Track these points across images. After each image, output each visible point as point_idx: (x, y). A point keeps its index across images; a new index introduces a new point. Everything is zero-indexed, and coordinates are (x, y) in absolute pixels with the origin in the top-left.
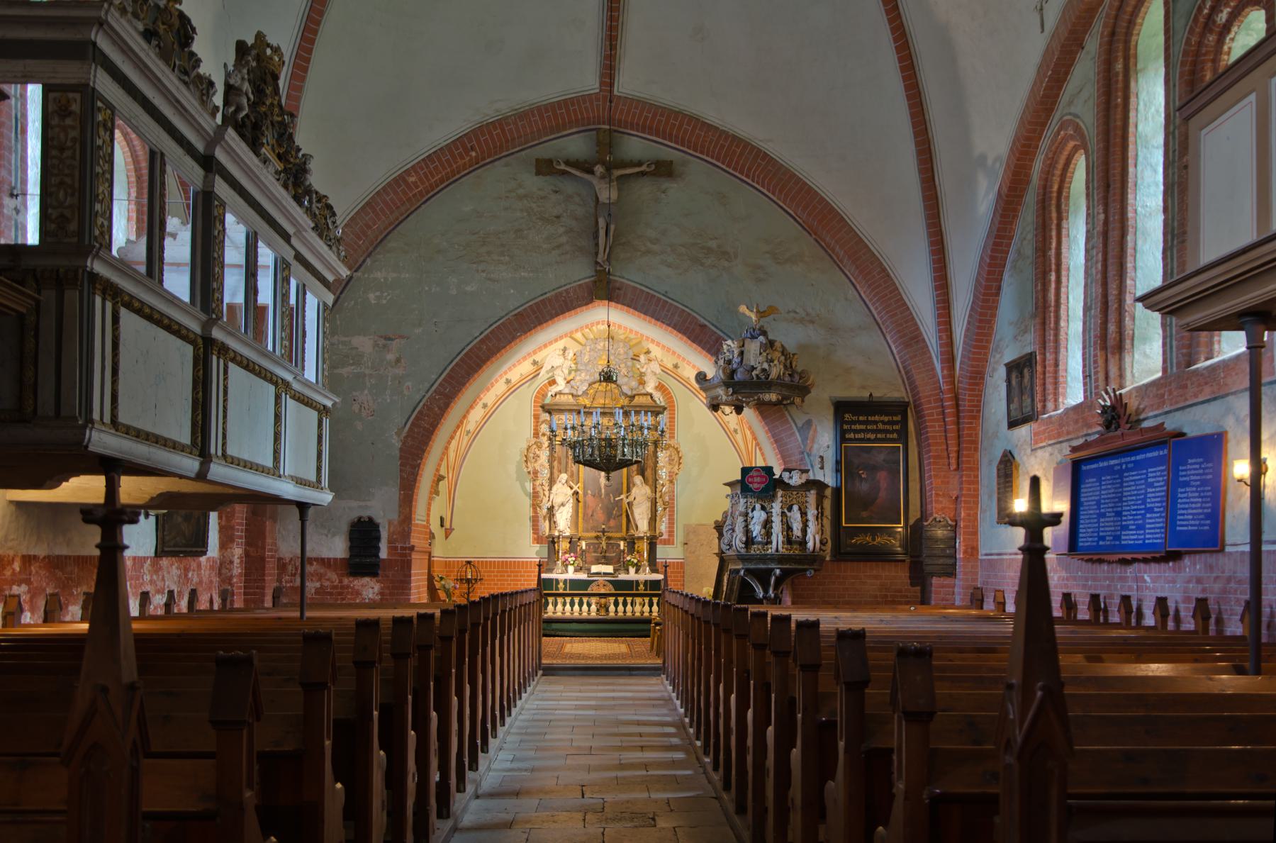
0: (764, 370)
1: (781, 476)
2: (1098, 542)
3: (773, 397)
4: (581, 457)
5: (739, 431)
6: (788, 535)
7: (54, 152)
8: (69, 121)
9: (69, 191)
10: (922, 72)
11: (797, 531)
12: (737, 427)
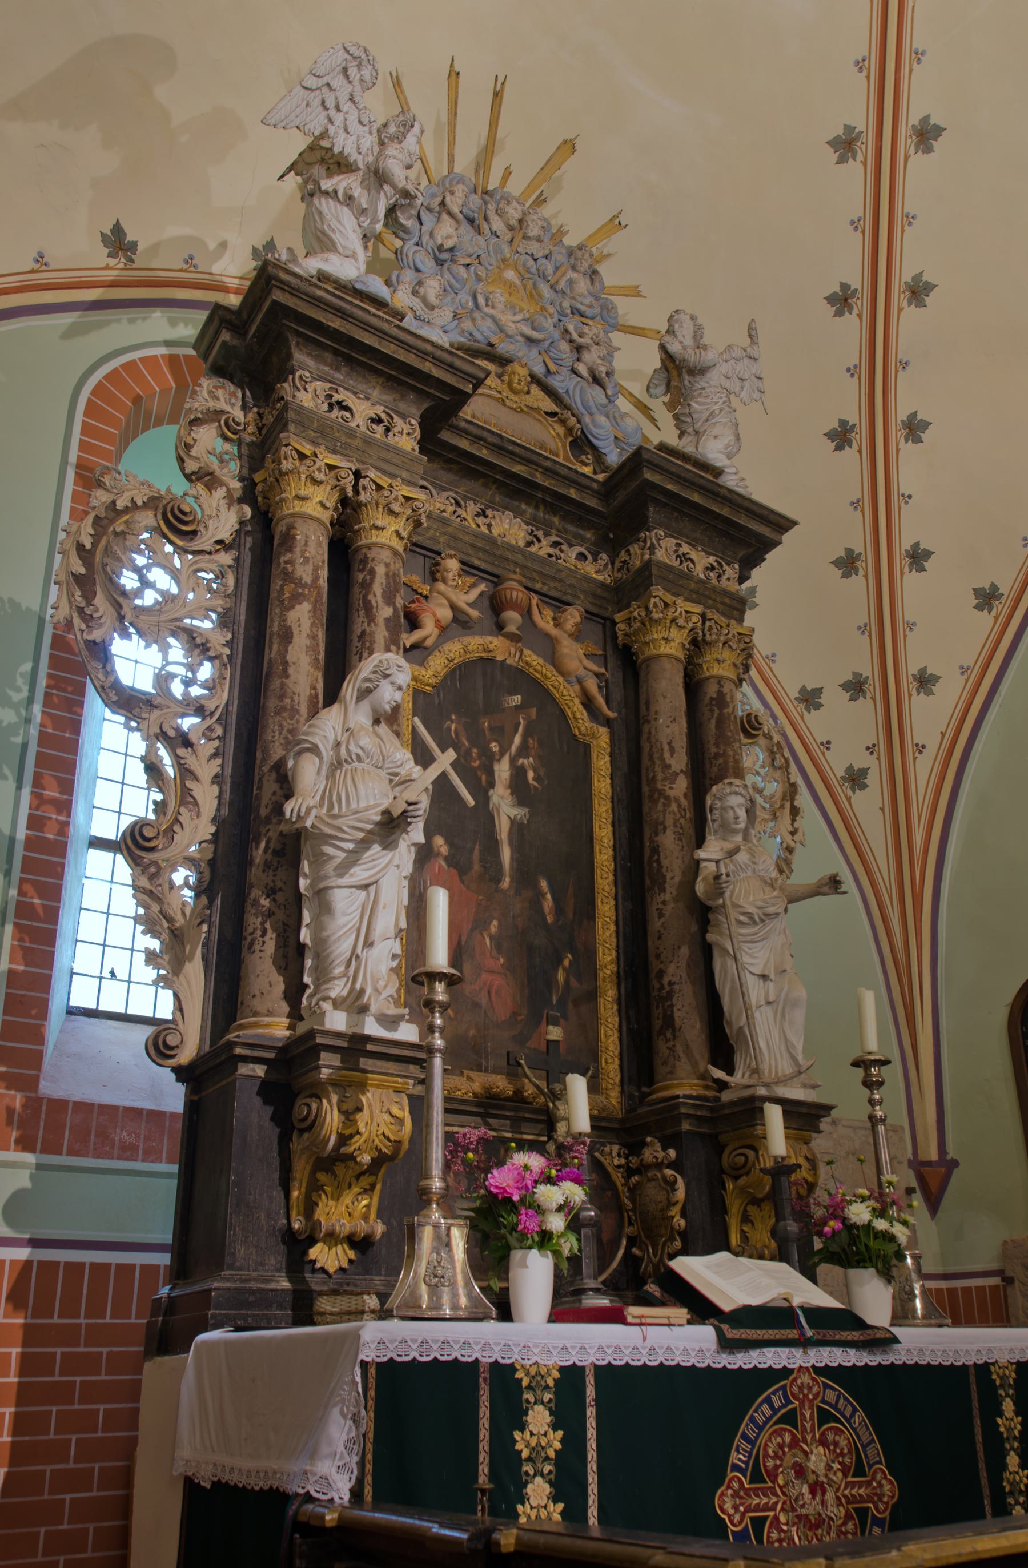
5: (872, 779)
12: (862, 760)
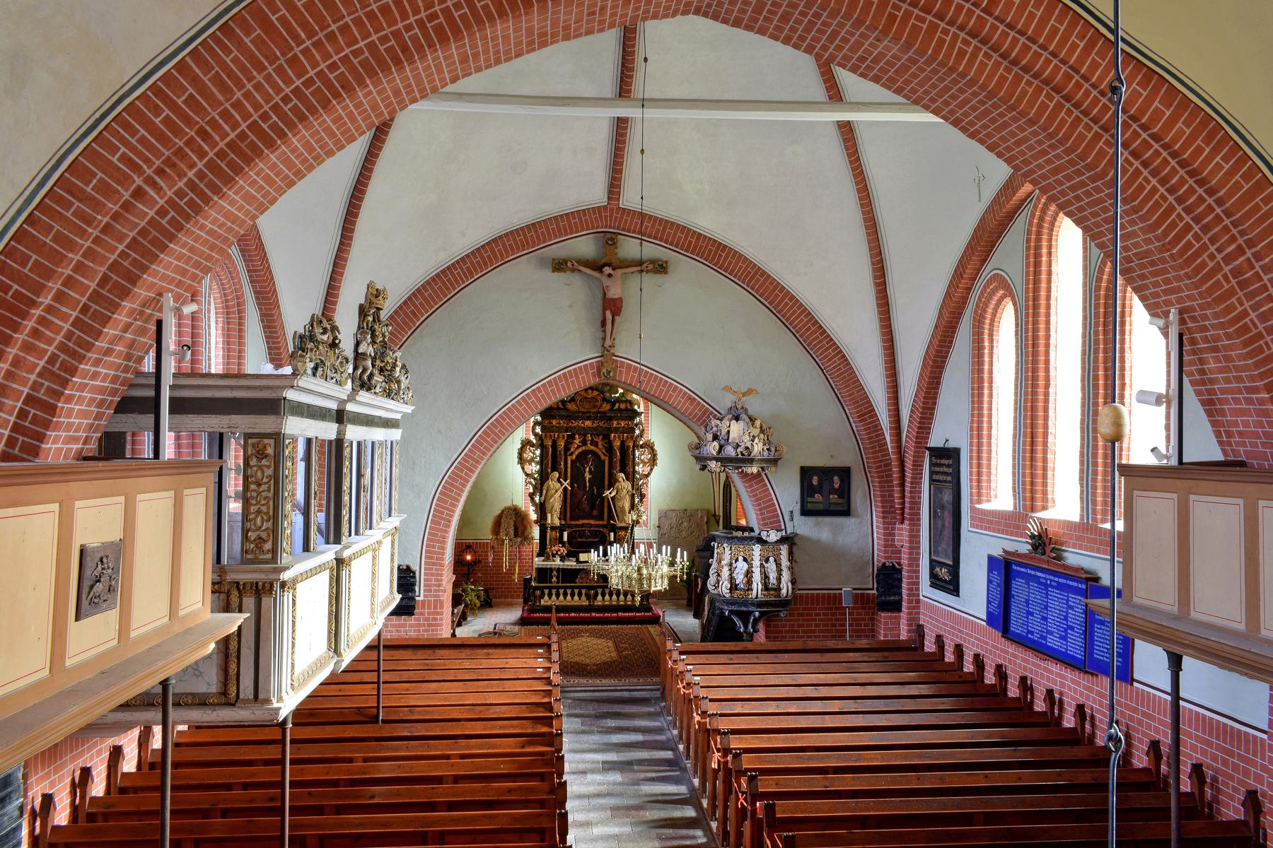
0: (747, 448)
1: (760, 534)
2: (1027, 634)
3: (754, 469)
4: (620, 585)
6: (765, 582)
7: (253, 487)
8: (264, 462)
9: (265, 517)
10: (845, 91)
11: (773, 576)
